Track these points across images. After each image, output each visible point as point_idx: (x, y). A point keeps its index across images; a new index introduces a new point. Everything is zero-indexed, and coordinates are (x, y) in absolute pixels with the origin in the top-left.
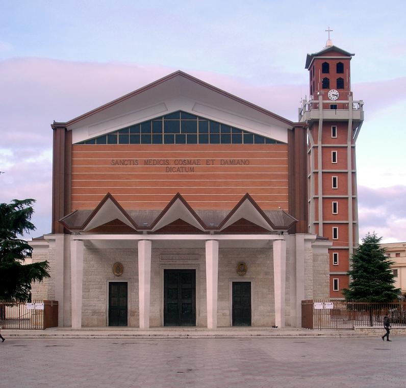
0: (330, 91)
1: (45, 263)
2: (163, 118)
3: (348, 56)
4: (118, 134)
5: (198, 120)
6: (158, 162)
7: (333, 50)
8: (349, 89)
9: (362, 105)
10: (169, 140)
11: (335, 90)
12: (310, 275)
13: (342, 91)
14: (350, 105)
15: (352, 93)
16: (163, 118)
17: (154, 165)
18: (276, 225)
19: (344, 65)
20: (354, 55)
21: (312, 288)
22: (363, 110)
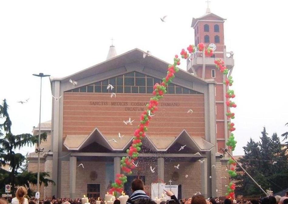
0: (210, 45)
1: (243, 148)
2: (124, 76)
3: (222, 20)
4: (94, 86)
5: (146, 77)
6: (120, 104)
7: (212, 16)
8: (223, 43)
9: (233, 55)
10: (127, 91)
11: (213, 44)
12: (220, 180)
13: (218, 45)
14: (224, 55)
15: (225, 46)
16: (124, 76)
17: (118, 105)
18: (165, 148)
19: (220, 27)
20: (226, 19)
21: (221, 188)
22: (225, 44)
